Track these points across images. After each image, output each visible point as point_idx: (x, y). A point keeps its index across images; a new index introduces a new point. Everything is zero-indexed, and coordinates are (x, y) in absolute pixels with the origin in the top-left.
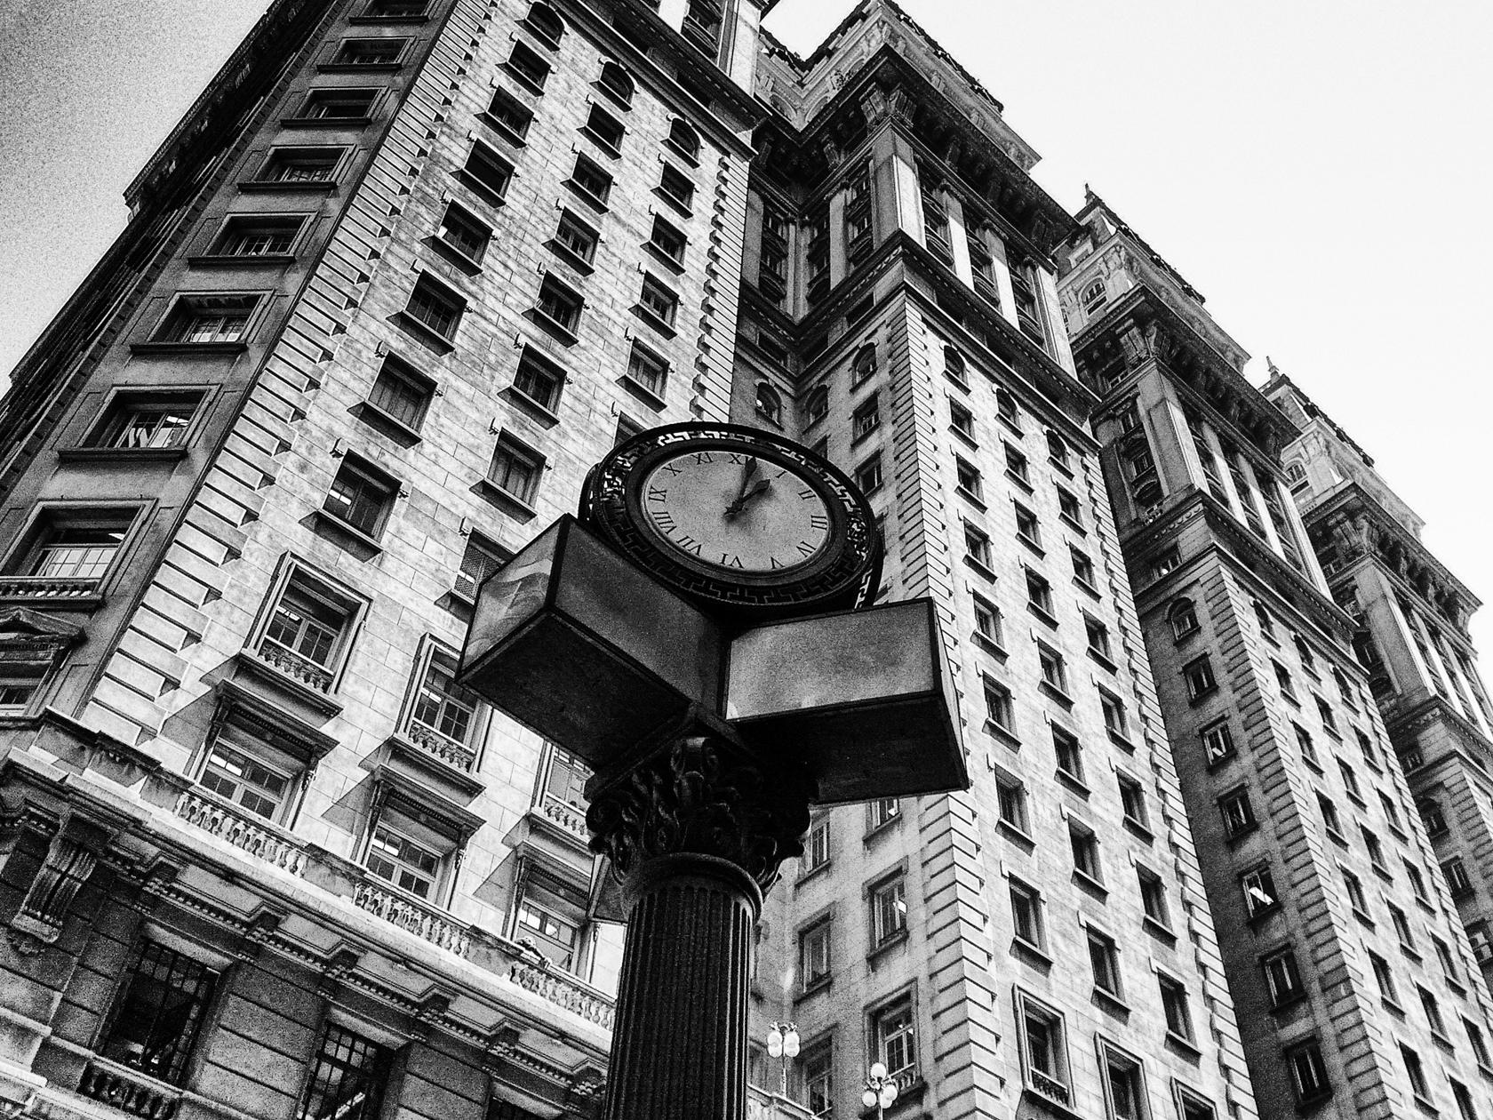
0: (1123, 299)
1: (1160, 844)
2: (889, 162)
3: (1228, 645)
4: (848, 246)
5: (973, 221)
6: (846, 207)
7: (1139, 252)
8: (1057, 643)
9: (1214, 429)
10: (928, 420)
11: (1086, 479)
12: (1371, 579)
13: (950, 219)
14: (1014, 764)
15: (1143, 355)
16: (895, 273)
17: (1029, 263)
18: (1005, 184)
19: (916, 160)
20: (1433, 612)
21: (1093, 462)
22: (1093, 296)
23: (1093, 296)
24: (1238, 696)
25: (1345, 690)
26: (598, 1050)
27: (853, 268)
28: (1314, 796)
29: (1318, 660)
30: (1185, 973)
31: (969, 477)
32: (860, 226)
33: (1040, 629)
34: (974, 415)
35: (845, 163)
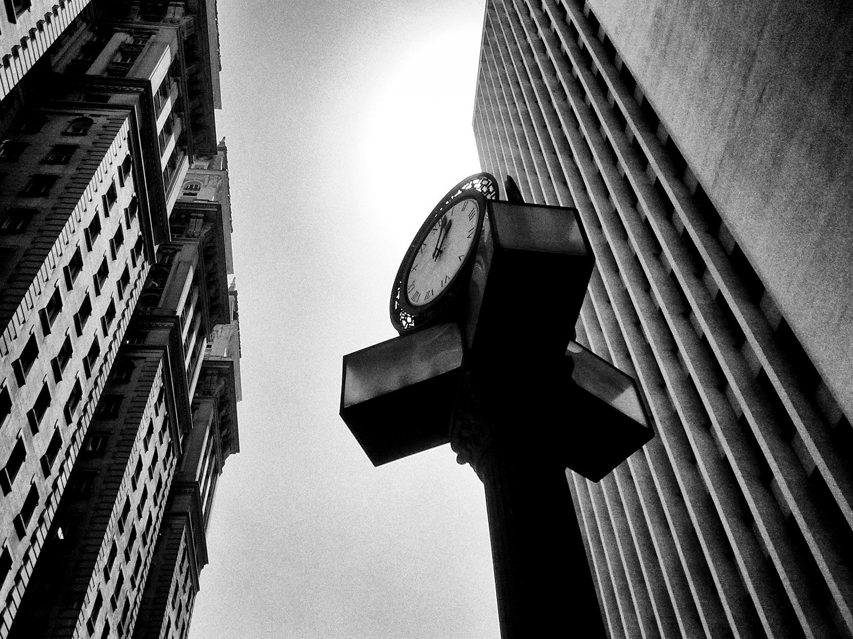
0: (206, 202)
1: (50, 480)
2: (164, 47)
3: (137, 399)
4: (111, 62)
5: (177, 108)
6: (123, 43)
7: (224, 188)
8: (75, 344)
9: (199, 293)
10: (98, 183)
11: (140, 274)
12: (208, 410)
13: (170, 97)
14: (14, 391)
15: (196, 235)
16: (130, 98)
17: (184, 150)
18: (201, 106)
19: (176, 56)
20: (219, 441)
21: (148, 267)
22: (191, 188)
23: (191, 188)
24: (124, 427)
25: (168, 455)
26: (805, 472)
27: (105, 75)
28: (126, 498)
29: (167, 433)
30: (17, 556)
31: (94, 229)
32: (124, 59)
33: (72, 332)
34: (117, 199)
35: (138, 23)
